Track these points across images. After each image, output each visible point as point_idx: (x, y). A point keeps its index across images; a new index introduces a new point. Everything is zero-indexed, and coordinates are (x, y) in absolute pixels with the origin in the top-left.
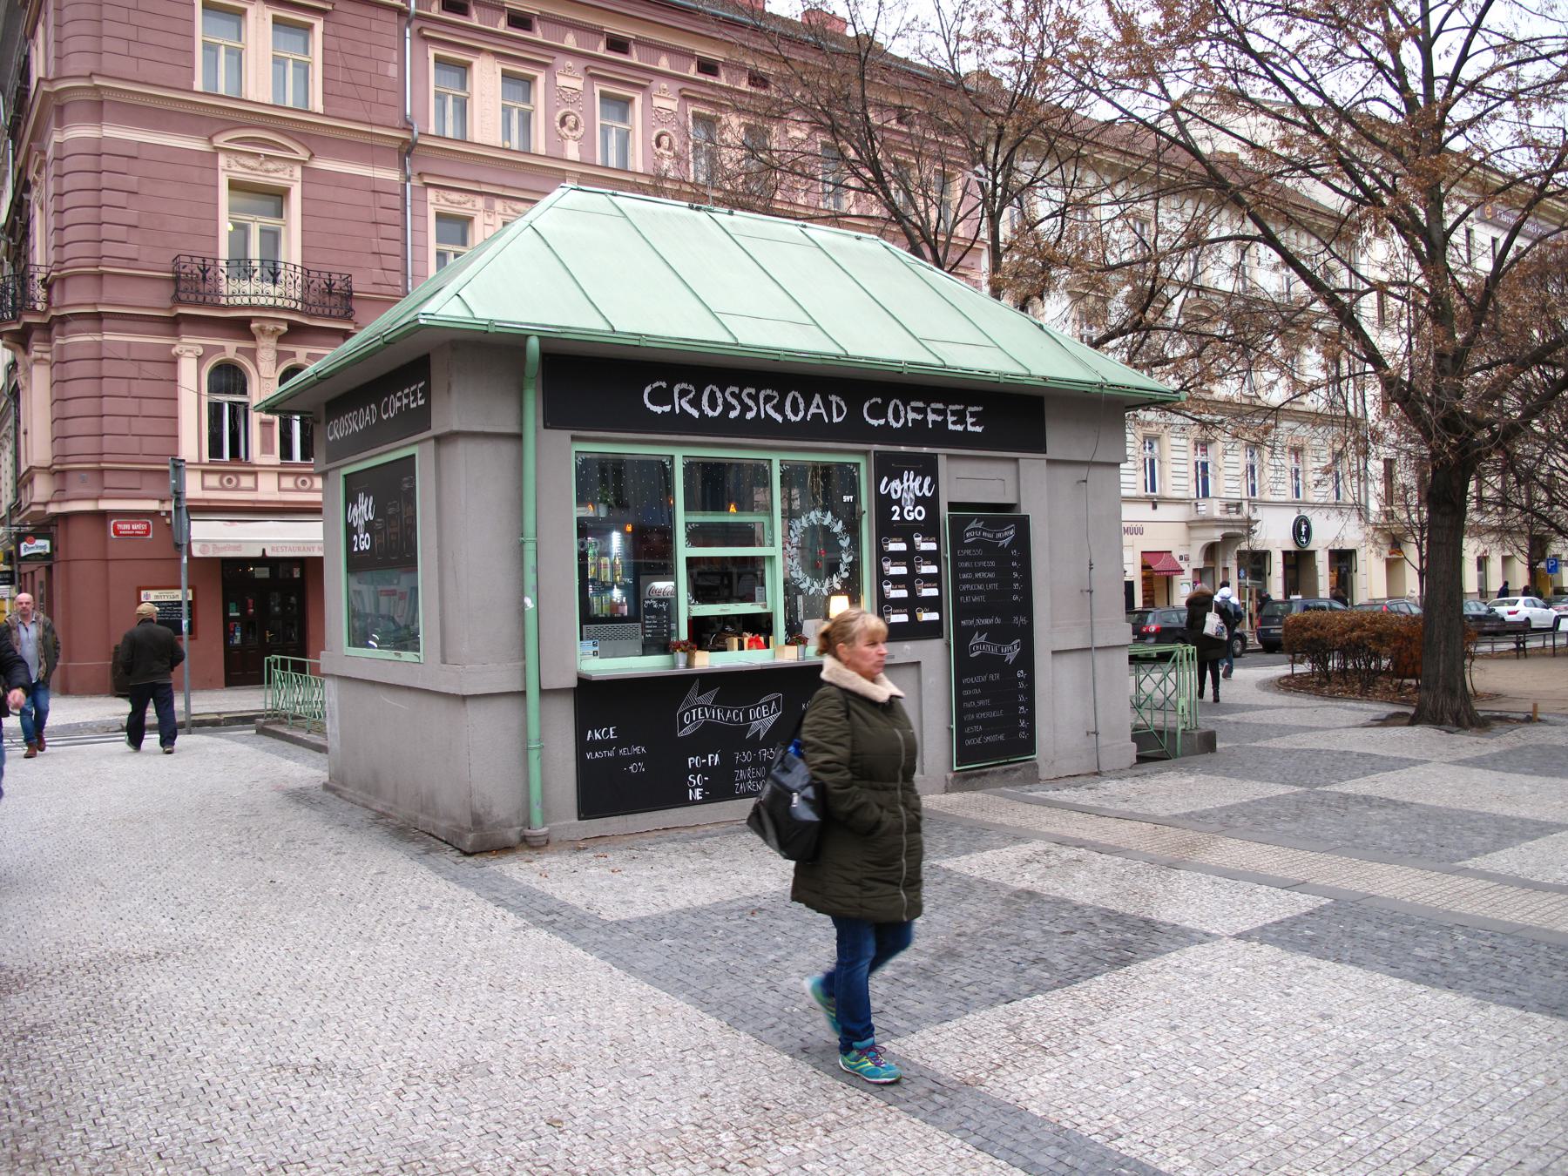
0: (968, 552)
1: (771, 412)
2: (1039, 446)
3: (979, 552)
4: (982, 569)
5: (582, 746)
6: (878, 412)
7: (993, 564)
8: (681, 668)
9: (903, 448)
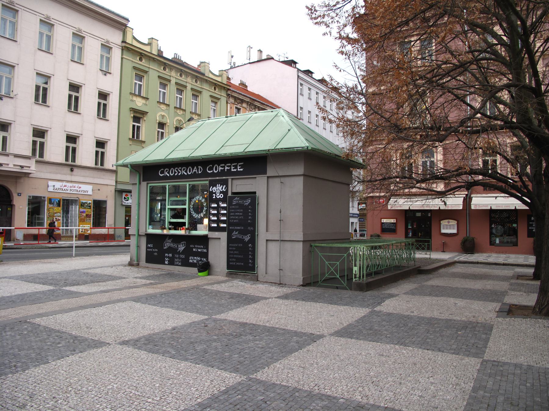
0: (234, 207)
1: (184, 173)
2: (265, 172)
3: (237, 207)
4: (238, 212)
5: (147, 248)
6: (162, 172)
7: (242, 210)
8: (187, 234)
9: (217, 178)
